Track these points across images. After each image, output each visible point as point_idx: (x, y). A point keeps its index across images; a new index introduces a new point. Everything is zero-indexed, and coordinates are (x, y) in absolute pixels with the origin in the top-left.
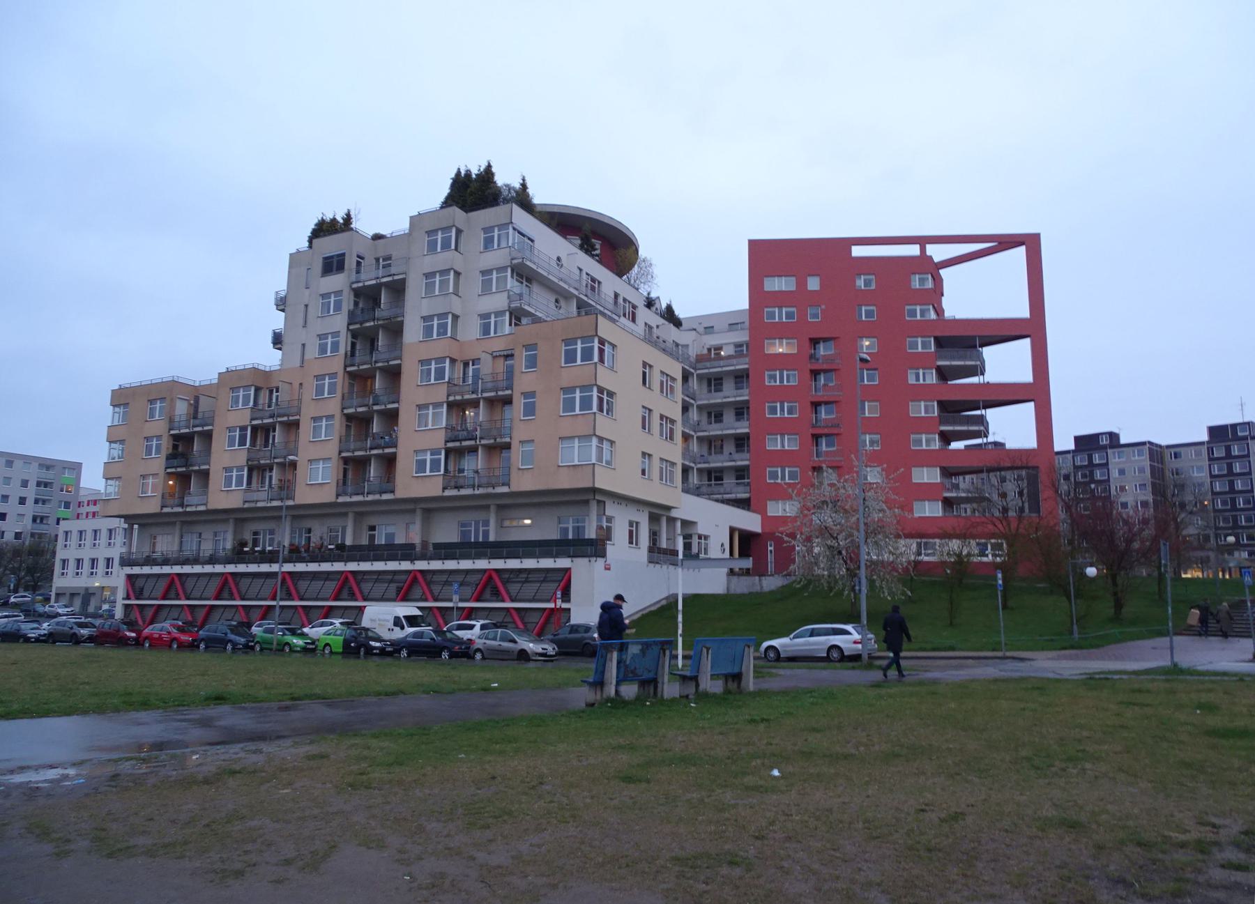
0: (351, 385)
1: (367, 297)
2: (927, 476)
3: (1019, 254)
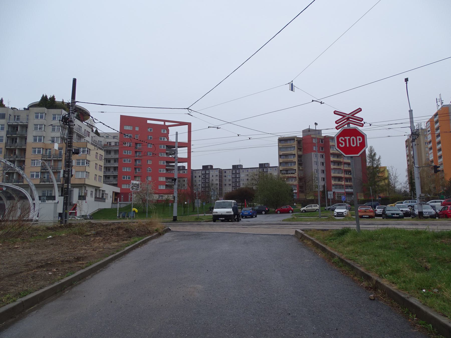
0: (7, 152)
1: (13, 128)
2: (162, 179)
3: (187, 126)
